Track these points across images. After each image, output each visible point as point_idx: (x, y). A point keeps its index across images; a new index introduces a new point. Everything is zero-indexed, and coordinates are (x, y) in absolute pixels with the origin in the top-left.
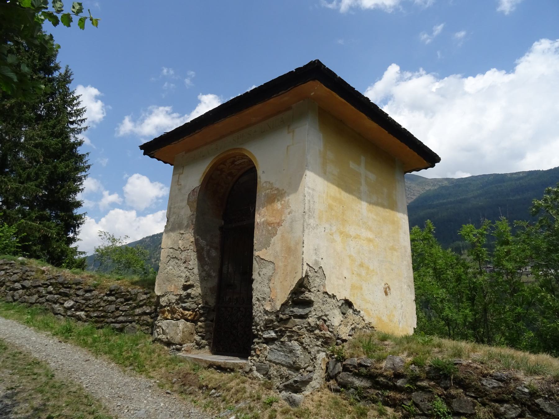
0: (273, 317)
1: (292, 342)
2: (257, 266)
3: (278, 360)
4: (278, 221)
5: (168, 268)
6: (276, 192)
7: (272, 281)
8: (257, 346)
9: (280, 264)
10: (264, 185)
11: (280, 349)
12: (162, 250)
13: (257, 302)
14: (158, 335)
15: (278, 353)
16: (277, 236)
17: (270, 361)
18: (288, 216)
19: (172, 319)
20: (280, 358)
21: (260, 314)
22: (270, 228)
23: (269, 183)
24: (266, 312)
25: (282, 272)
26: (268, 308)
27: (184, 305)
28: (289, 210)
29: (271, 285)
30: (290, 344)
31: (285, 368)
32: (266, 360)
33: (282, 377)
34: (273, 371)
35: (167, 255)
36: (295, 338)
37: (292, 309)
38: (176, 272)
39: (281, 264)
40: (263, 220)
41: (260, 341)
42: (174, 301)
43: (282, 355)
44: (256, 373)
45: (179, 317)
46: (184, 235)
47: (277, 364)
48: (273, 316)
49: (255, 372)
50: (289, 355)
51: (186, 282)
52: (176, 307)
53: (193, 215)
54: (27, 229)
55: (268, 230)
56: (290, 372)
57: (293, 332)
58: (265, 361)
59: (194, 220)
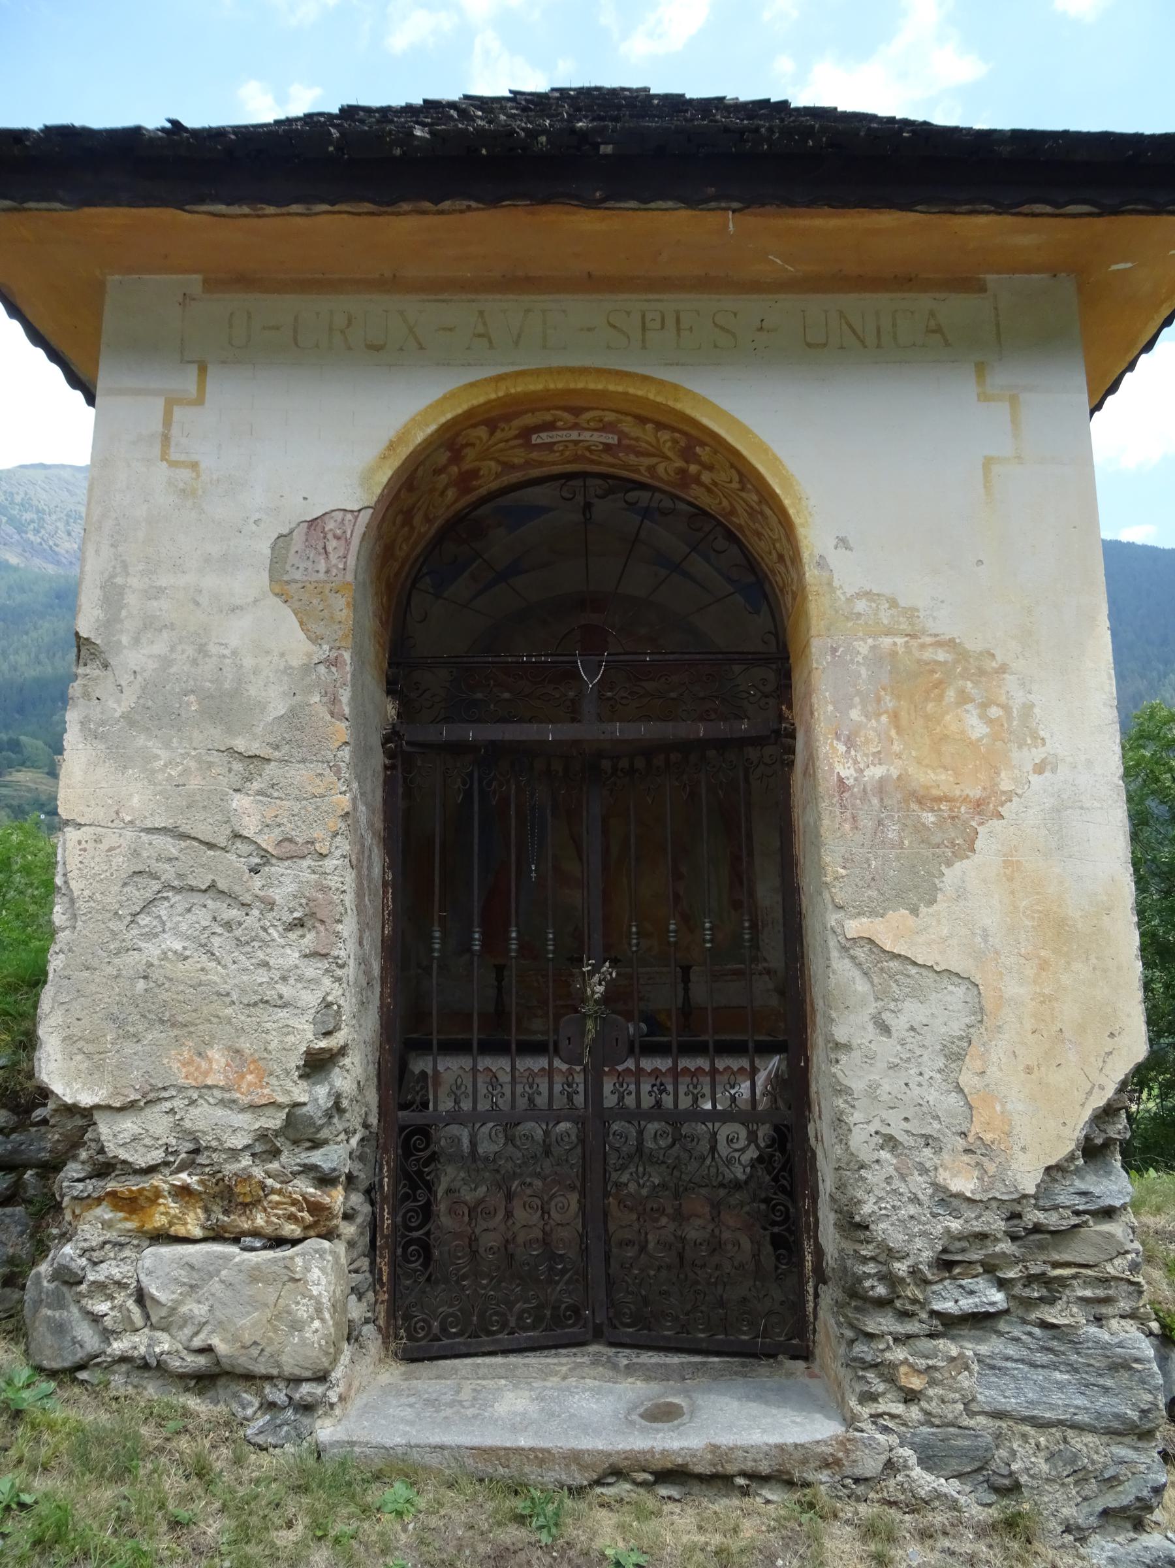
0: (996, 1223)
1: (1114, 1323)
2: (861, 986)
3: (1052, 1406)
4: (976, 793)
5: (152, 950)
6: (941, 656)
7: (972, 1063)
8: (899, 1354)
9: (1015, 988)
10: (861, 606)
11: (1040, 1358)
12: (71, 834)
13: (884, 1155)
14: (107, 1335)
15: (1039, 1375)
16: (976, 859)
17: (998, 1415)
18: (1034, 778)
19: (216, 1235)
20: (1057, 1398)
21: (912, 1210)
22: (929, 818)
23: (893, 603)
24: (947, 1200)
25: (1028, 1025)
26: (964, 1184)
27: (316, 1157)
28: (1038, 754)
29: (967, 1079)
30: (1105, 1336)
31: (1089, 1438)
32: (972, 1414)
33: (1081, 1476)
34: (1026, 1457)
35: (121, 864)
36: (1124, 1305)
37: (1080, 1185)
38: (232, 971)
39: (1013, 989)
40: (877, 772)
41: (912, 1327)
42: (238, 1141)
43: (1061, 1386)
44: (926, 1481)
45: (291, 1229)
46: (271, 769)
47: (1040, 1424)
48: (988, 1216)
49: (917, 1472)
50: (1109, 1383)
51: (328, 1034)
52: (258, 1173)
53: (332, 663)
54: (1008, 872)
55: (919, 829)
56: (1116, 1450)
57: (1105, 1281)
58: (967, 1422)
59: (345, 696)
